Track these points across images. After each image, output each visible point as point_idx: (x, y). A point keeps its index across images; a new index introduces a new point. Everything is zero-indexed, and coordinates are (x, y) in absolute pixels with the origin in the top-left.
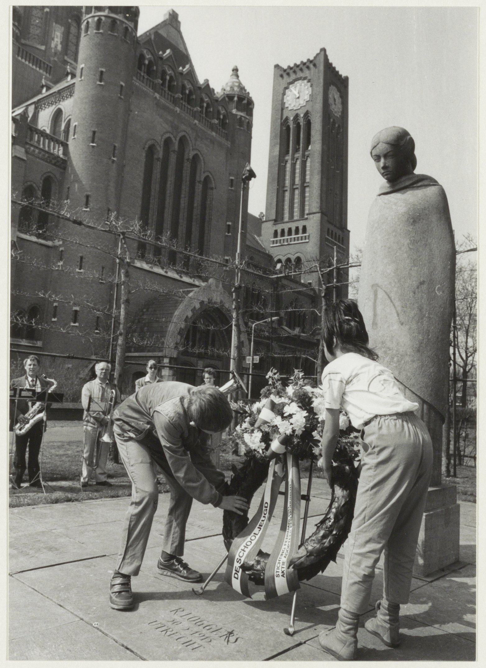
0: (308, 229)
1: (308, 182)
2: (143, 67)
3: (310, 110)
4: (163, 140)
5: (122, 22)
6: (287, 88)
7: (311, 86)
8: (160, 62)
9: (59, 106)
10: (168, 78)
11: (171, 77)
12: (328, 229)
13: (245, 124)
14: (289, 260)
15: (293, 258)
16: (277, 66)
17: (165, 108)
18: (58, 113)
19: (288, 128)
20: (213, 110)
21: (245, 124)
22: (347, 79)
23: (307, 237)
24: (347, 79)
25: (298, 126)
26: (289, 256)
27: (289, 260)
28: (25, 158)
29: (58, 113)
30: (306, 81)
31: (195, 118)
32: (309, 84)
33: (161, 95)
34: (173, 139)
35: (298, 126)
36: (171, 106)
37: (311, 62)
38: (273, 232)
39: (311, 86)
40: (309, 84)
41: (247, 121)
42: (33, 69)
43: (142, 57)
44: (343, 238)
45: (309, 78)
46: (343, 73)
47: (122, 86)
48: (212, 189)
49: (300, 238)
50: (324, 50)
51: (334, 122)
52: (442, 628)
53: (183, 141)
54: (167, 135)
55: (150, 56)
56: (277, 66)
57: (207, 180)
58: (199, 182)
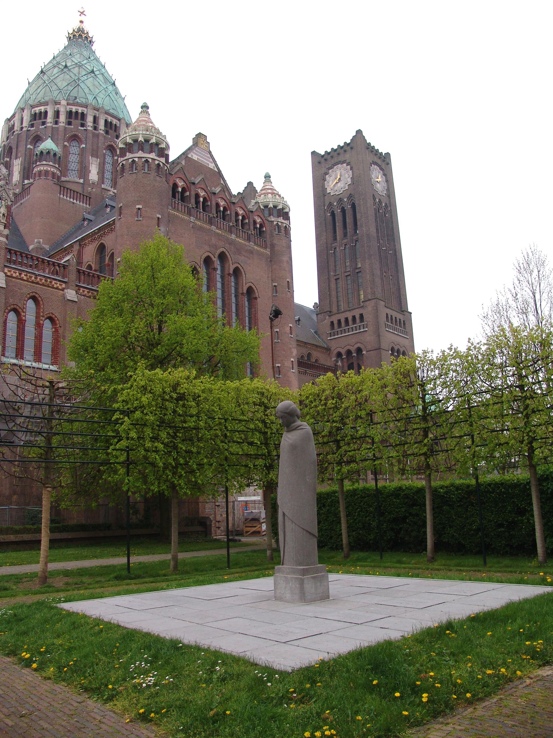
0: (365, 317)
1: (360, 268)
2: (177, 194)
3: (352, 193)
4: (202, 260)
5: (153, 160)
6: (326, 174)
7: (351, 169)
8: (193, 187)
9: (102, 241)
10: (201, 199)
11: (205, 199)
12: (387, 314)
13: (283, 229)
14: (349, 352)
15: (353, 349)
16: (314, 153)
17: (201, 228)
18: (102, 248)
19: (333, 214)
20: (249, 221)
21: (283, 229)
22: (388, 154)
23: (365, 326)
24: (388, 154)
25: (343, 211)
26: (348, 347)
27: (349, 352)
28: (76, 300)
29: (102, 248)
30: (345, 165)
31: (231, 232)
32: (349, 167)
33: (196, 218)
34: (212, 257)
35: (343, 211)
36: (207, 226)
37: (349, 144)
38: (330, 323)
39: (351, 169)
40: (349, 167)
41: (284, 225)
42: (74, 203)
43: (175, 186)
44: (404, 321)
45: (348, 161)
46: (383, 150)
47: (158, 218)
48: (256, 298)
49: (358, 328)
50: (359, 132)
51: (380, 201)
52: (403, 633)
53: (222, 257)
54: (207, 254)
55: (182, 183)
56: (314, 153)
57: (250, 291)
58: (243, 294)
